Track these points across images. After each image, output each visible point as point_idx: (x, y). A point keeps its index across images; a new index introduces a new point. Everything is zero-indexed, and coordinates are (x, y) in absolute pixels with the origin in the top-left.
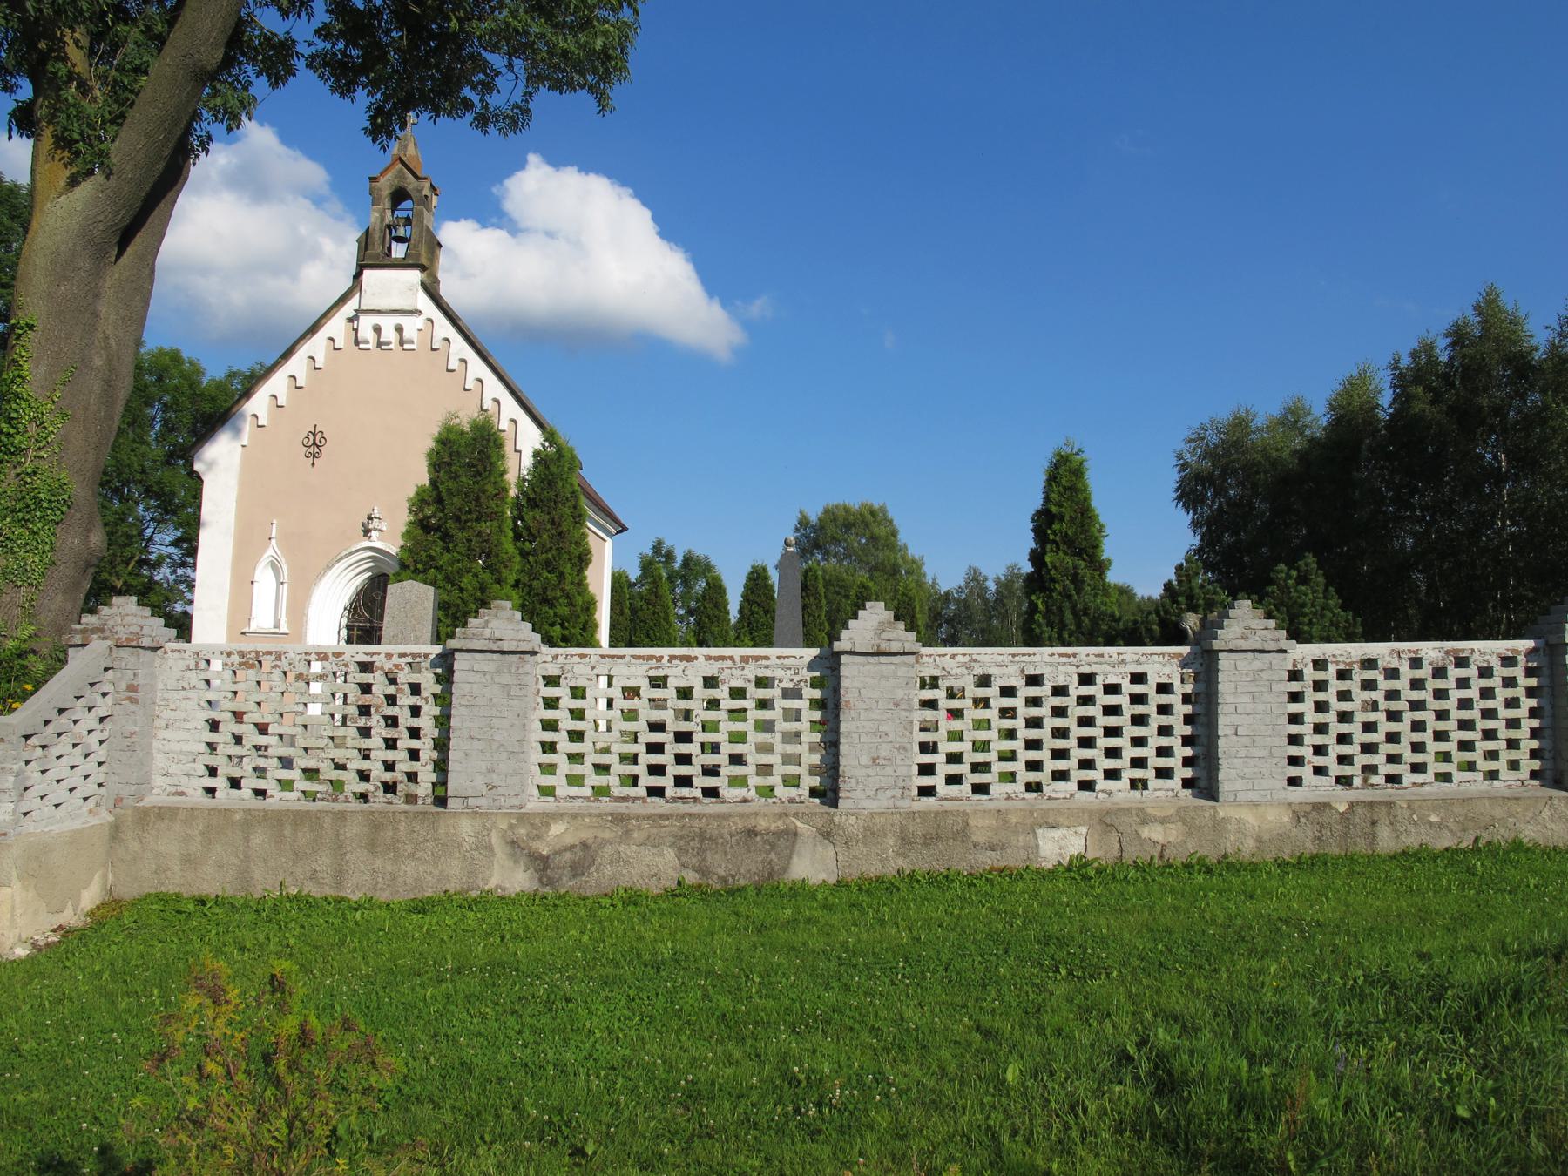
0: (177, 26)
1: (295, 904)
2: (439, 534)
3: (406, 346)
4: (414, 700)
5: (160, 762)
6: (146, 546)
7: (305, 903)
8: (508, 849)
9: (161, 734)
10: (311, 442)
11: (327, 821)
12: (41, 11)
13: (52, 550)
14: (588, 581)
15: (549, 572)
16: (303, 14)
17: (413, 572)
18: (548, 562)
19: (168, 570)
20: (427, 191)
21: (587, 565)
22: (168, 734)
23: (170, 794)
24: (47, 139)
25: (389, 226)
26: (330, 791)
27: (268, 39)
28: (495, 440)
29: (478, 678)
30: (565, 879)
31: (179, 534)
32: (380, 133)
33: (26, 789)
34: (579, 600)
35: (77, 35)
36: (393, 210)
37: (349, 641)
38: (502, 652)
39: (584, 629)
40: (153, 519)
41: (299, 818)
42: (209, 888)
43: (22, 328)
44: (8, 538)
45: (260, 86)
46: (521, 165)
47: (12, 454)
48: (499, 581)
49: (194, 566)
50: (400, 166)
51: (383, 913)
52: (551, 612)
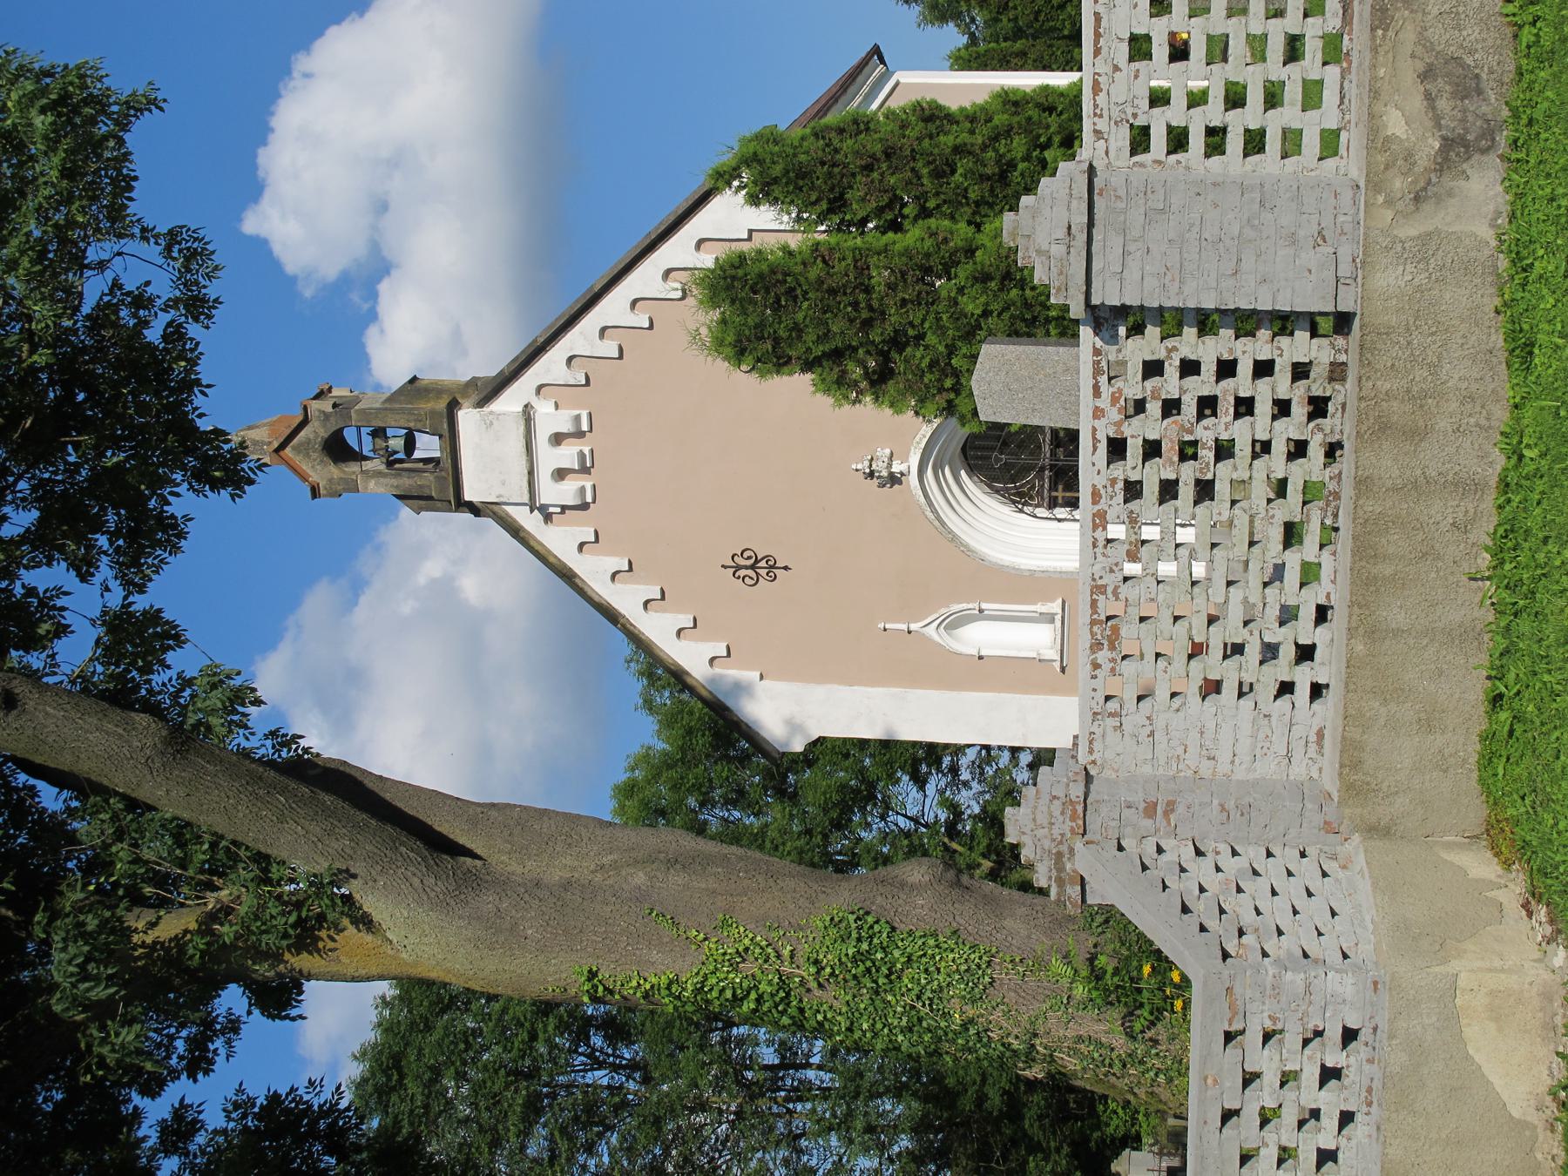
0: (105, 782)
1: (1507, 556)
2: (894, 355)
3: (585, 427)
4: (1172, 370)
5: (1268, 768)
6: (926, 826)
7: (1508, 539)
8: (1427, 207)
9: (1223, 767)
10: (750, 572)
11: (1370, 506)
12: (110, 977)
13: (935, 935)
14: (967, 104)
15: (953, 172)
16: (59, 603)
17: (958, 393)
18: (938, 174)
19: (964, 792)
20: (325, 405)
21: (940, 107)
22: (1224, 757)
23: (1320, 752)
24: (303, 961)
25: (390, 464)
26: (1321, 504)
27: (110, 651)
28: (733, 266)
29: (1133, 265)
30: (1485, 109)
31: (906, 778)
32: (237, 472)
33: (1306, 956)
34: (1000, 119)
35: (141, 925)
36: (359, 457)
37: (1073, 504)
38: (1091, 224)
39: (1050, 109)
40: (883, 817)
41: (1363, 551)
42: (1475, 689)
43: (595, 987)
44: (919, 997)
45: (183, 661)
46: (261, 245)
47: (788, 994)
48: (970, 252)
49: (959, 750)
50: (288, 450)
51: (1528, 413)
52: (1021, 166)
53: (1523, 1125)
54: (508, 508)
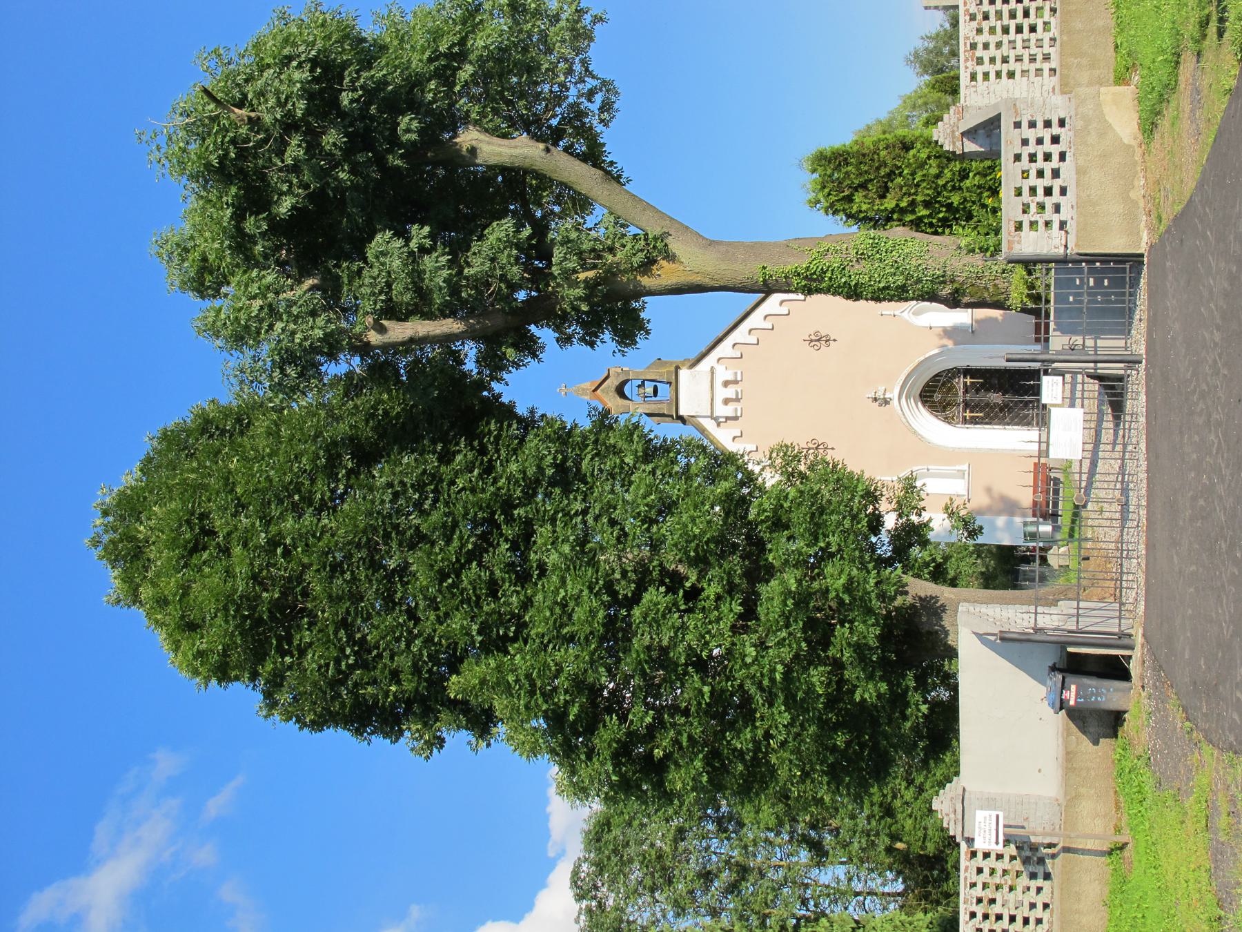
53: (1130, 146)
54: (701, 420)
